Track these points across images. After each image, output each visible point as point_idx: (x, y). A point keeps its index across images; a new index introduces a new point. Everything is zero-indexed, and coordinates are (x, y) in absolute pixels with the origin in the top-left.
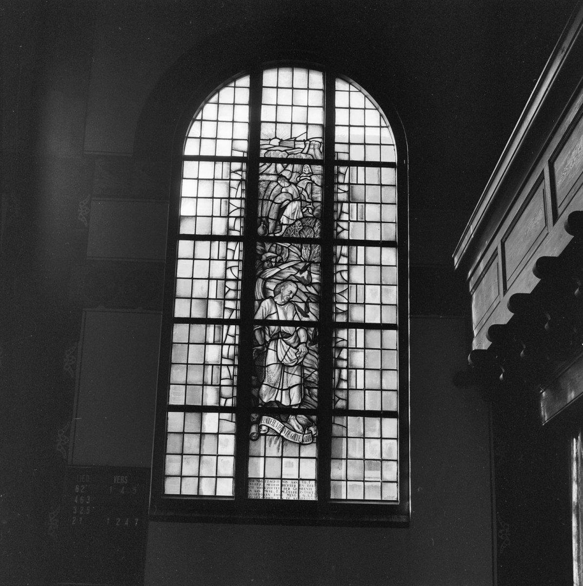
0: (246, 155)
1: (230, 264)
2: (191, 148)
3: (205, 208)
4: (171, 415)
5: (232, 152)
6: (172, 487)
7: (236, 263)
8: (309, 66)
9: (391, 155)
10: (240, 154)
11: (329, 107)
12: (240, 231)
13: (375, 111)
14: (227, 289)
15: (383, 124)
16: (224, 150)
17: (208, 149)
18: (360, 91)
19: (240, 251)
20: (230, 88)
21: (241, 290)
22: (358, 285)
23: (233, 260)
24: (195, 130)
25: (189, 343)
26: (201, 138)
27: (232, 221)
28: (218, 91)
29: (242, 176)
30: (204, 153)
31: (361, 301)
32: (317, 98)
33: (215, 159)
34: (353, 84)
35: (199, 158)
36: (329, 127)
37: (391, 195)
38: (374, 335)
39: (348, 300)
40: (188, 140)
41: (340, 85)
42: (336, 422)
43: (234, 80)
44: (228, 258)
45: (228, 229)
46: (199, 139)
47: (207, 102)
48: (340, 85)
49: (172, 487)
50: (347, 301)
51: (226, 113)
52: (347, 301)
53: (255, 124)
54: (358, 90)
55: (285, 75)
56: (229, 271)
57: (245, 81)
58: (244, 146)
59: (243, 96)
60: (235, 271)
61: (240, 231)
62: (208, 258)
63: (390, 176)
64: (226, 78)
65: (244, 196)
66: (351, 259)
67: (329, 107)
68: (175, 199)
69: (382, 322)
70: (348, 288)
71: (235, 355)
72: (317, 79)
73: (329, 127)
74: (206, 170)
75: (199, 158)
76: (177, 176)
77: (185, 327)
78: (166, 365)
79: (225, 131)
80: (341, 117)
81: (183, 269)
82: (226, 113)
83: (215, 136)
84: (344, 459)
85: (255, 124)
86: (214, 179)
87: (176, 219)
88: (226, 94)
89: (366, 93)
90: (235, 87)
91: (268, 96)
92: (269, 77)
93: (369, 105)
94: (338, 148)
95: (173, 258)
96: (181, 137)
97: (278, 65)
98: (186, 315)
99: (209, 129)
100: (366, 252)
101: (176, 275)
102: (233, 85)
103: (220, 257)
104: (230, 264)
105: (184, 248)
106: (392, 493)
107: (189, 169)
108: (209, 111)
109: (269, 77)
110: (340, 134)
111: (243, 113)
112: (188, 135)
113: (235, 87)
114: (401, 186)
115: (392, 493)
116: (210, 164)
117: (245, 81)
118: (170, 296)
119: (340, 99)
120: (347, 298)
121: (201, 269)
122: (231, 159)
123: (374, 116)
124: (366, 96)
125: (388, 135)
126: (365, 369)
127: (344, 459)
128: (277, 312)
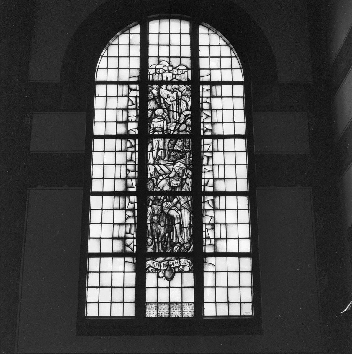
2: (100, 75)
6: (92, 311)
8: (181, 18)
9: (239, 76)
10: (135, 79)
14: (127, 216)
15: (233, 55)
16: (124, 76)
17: (112, 76)
20: (127, 101)
21: (139, 103)
24: (102, 63)
26: (106, 97)
27: (129, 181)
29: (136, 132)
30: (104, 250)
34: (211, 29)
36: (195, 57)
37: (240, 103)
43: (129, 29)
45: (127, 186)
46: (103, 166)
48: (202, 30)
49: (92, 311)
51: (123, 51)
52: (213, 218)
53: (144, 57)
54: (214, 33)
57: (137, 29)
58: (137, 73)
59: (136, 39)
68: (90, 109)
72: (186, 27)
73: (195, 57)
74: (112, 89)
76: (92, 95)
80: (203, 51)
83: (116, 120)
85: (144, 57)
86: (115, 179)
88: (124, 38)
90: (130, 34)
92: (153, 26)
93: (222, 42)
95: (89, 150)
96: (93, 68)
97: (160, 18)
98: (102, 133)
100: (242, 308)
102: (128, 32)
103: (122, 149)
106: (248, 310)
108: (113, 50)
109: (153, 26)
110: (203, 63)
111: (136, 51)
112: (92, 177)
113: (130, 34)
114: (247, 98)
116: (115, 86)
117: (137, 29)
119: (203, 39)
123: (226, 51)
124: (220, 37)
125: (236, 63)
126: (224, 165)
128: (161, 169)
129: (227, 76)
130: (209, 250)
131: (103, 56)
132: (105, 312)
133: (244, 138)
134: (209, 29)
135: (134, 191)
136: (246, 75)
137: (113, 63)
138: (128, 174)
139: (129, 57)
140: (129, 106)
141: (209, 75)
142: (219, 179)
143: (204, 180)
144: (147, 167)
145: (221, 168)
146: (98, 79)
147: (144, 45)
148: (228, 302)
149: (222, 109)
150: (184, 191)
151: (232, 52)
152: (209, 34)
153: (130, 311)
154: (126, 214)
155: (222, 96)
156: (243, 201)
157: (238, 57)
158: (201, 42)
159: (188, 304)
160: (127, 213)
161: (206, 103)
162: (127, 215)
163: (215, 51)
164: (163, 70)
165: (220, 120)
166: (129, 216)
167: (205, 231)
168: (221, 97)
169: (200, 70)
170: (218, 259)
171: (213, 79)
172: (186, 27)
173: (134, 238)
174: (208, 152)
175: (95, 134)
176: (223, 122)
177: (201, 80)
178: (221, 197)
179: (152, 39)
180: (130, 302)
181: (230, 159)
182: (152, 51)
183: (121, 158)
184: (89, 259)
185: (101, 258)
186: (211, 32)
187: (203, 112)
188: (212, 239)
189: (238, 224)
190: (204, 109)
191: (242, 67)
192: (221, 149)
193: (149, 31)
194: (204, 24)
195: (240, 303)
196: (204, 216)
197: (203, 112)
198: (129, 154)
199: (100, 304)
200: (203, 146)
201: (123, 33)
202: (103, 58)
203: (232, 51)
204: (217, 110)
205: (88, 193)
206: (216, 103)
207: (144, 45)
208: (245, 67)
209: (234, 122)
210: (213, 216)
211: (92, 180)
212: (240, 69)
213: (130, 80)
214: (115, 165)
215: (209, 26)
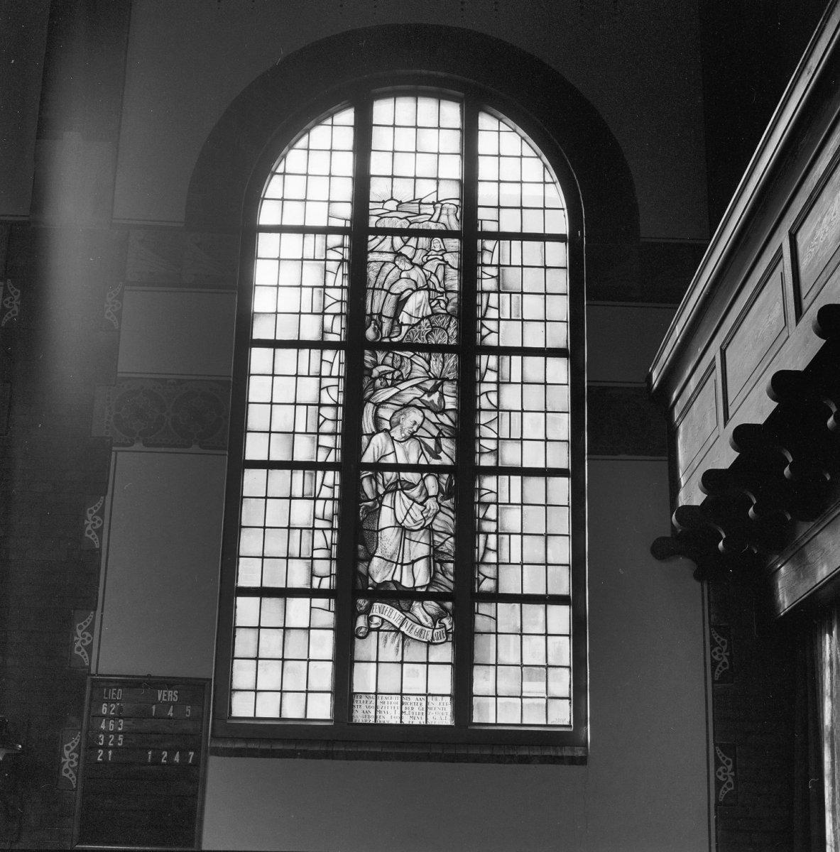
0: (348, 224)
1: (326, 382)
2: (268, 214)
3: (289, 300)
7: (334, 381)
9: (559, 223)
10: (341, 224)
12: (340, 335)
13: (536, 159)
14: (321, 419)
15: (548, 179)
17: (293, 216)
18: (515, 131)
23: (330, 376)
24: (274, 187)
28: (308, 131)
32: (452, 141)
36: (469, 184)
37: (560, 281)
38: (536, 484)
41: (486, 122)
43: (332, 115)
47: (291, 148)
48: (486, 122)
49: (242, 707)
50: (496, 436)
51: (319, 163)
53: (362, 180)
54: (511, 130)
56: (324, 392)
57: (347, 117)
60: (333, 392)
61: (340, 335)
63: (558, 254)
64: (318, 111)
65: (346, 283)
68: (245, 288)
70: (498, 417)
71: (333, 514)
73: (469, 184)
78: (233, 528)
79: (318, 189)
80: (486, 168)
81: (257, 389)
82: (319, 163)
85: (362, 180)
87: (246, 318)
88: (319, 135)
89: (524, 134)
91: (381, 138)
92: (382, 110)
94: (482, 214)
95: (242, 374)
96: (254, 199)
98: (262, 456)
99: (294, 187)
104: (326, 382)
105: (259, 359)
106: (562, 715)
107: (266, 244)
108: (294, 159)
109: (382, 110)
110: (486, 193)
111: (345, 164)
115: (562, 715)
117: (347, 117)
118: (239, 429)
119: (486, 142)
121: (284, 390)
124: (523, 138)
125: (555, 195)
126: (522, 534)
130: (487, 461)
132: (267, 708)
135: (339, 340)
138: (322, 424)
145: (516, 540)
146: (255, 337)
147: (363, 147)
148: (521, 634)
150: (442, 231)
153: (321, 709)
154: (319, 414)
155: (522, 291)
158: (482, 174)
159: (440, 697)
160: (321, 412)
161: (487, 575)
162: (321, 417)
165: (516, 261)
166: (326, 419)
170: (502, 607)
171: (504, 229)
175: (260, 223)
177: (476, 591)
178: (512, 477)
180: (321, 626)
183: (312, 275)
184: (263, 204)
187: (482, 324)
188: (490, 536)
189: (544, 208)
194: (490, 109)
197: (482, 324)
198: (328, 319)
199: (271, 373)
201: (319, 123)
203: (546, 170)
204: (510, 411)
205: (239, 465)
206: (510, 397)
207: (363, 147)
209: (547, 564)
211: (233, 662)
214: (295, 404)
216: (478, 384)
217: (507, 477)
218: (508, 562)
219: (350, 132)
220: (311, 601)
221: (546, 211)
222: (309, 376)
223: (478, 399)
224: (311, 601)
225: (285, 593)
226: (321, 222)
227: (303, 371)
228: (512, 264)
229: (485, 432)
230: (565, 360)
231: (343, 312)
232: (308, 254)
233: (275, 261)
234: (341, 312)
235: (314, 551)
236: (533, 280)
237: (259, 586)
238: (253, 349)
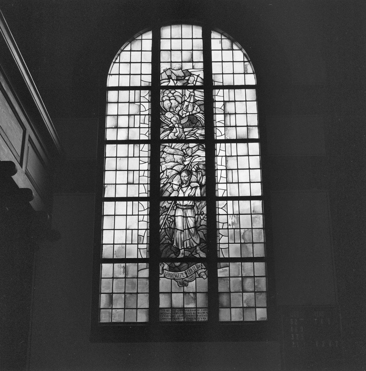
0: (150, 85)
2: (112, 81)
3: (120, 237)
4: (108, 147)
5: (140, 124)
9: (251, 80)
10: (147, 84)
11: (207, 51)
12: (148, 125)
13: (239, 51)
16: (136, 82)
17: (125, 82)
19: (147, 237)
22: (233, 170)
24: (114, 68)
25: (115, 215)
31: (235, 180)
33: (127, 142)
35: (119, 89)
39: (227, 212)
40: (106, 172)
41: (214, 35)
42: (217, 100)
43: (141, 34)
44: (139, 245)
48: (214, 35)
49: (104, 318)
50: (226, 213)
52: (226, 213)
53: (156, 62)
55: (176, 30)
58: (149, 79)
61: (148, 125)
62: (125, 228)
66: (228, 179)
67: (207, 51)
69: (250, 201)
70: (227, 204)
72: (198, 31)
75: (119, 89)
76: (104, 103)
77: (116, 92)
80: (215, 56)
84: (221, 37)
92: (166, 32)
96: (105, 73)
98: (113, 195)
101: (105, 169)
102: (140, 38)
108: (124, 56)
109: (166, 32)
110: (216, 68)
111: (148, 56)
115: (261, 314)
116: (125, 146)
119: (215, 44)
120: (226, 211)
121: (120, 222)
122: (140, 88)
123: (239, 55)
127: (221, 37)
129: (239, 80)
131: (115, 63)
133: (260, 200)
134: (222, 34)
136: (258, 79)
137: (124, 69)
139: (141, 51)
140: (141, 112)
141: (224, 135)
142: (229, 101)
143: (218, 216)
144: (160, 105)
147: (156, 51)
149: (235, 114)
151: (245, 57)
152: (221, 39)
156: (251, 94)
157: (251, 62)
163: (227, 55)
164: (175, 83)
165: (234, 154)
167: (219, 251)
168: (236, 126)
169: (212, 51)
172: (198, 31)
173: (148, 128)
174: (221, 170)
176: (235, 101)
178: (234, 201)
179: (165, 45)
181: (241, 107)
182: (164, 57)
185: (118, 86)
186: (223, 37)
187: (216, 129)
190: (216, 100)
191: (254, 72)
192: (234, 154)
193: (159, 304)
195: (248, 155)
196: (217, 189)
197: (216, 129)
200: (218, 237)
202: (115, 64)
204: (232, 170)
207: (156, 51)
208: (257, 72)
210: (226, 189)
212: (253, 73)
213: (140, 196)
215: (221, 32)
216: (216, 157)
217: (228, 90)
218: (232, 182)
219: (150, 42)
220: (141, 85)
221: (251, 184)
222: (134, 171)
223: (216, 151)
224: (141, 85)
225: (127, 142)
226: (138, 84)
227: (130, 213)
228: (232, 155)
229: (221, 211)
230: (255, 90)
231: (149, 156)
232: (132, 100)
233: (116, 104)
234: (148, 169)
235: (139, 222)
236: (241, 107)
237: (116, 139)
238: (107, 145)
